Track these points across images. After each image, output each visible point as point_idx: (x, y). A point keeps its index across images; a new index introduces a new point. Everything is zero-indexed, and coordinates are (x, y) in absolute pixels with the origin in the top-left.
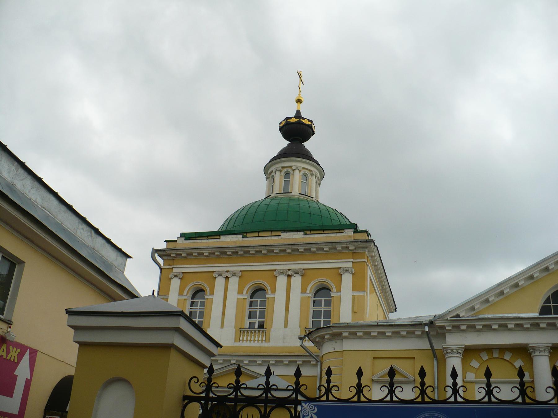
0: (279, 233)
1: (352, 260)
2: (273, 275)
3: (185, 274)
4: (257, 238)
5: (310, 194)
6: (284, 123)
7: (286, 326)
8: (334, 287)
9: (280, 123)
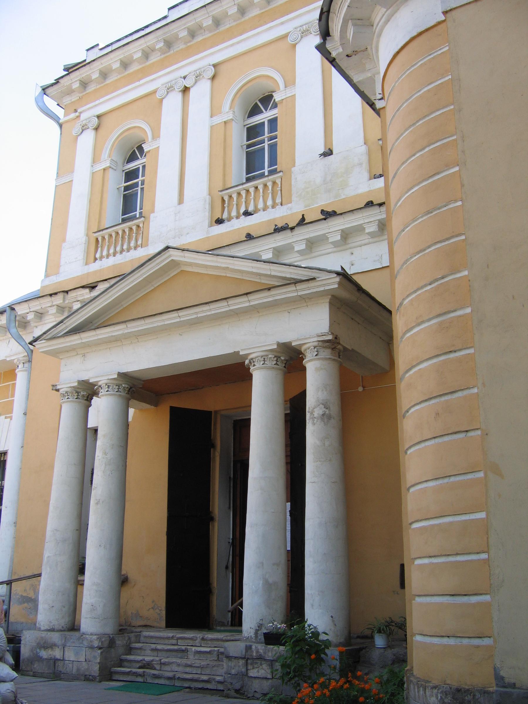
7: (181, 201)
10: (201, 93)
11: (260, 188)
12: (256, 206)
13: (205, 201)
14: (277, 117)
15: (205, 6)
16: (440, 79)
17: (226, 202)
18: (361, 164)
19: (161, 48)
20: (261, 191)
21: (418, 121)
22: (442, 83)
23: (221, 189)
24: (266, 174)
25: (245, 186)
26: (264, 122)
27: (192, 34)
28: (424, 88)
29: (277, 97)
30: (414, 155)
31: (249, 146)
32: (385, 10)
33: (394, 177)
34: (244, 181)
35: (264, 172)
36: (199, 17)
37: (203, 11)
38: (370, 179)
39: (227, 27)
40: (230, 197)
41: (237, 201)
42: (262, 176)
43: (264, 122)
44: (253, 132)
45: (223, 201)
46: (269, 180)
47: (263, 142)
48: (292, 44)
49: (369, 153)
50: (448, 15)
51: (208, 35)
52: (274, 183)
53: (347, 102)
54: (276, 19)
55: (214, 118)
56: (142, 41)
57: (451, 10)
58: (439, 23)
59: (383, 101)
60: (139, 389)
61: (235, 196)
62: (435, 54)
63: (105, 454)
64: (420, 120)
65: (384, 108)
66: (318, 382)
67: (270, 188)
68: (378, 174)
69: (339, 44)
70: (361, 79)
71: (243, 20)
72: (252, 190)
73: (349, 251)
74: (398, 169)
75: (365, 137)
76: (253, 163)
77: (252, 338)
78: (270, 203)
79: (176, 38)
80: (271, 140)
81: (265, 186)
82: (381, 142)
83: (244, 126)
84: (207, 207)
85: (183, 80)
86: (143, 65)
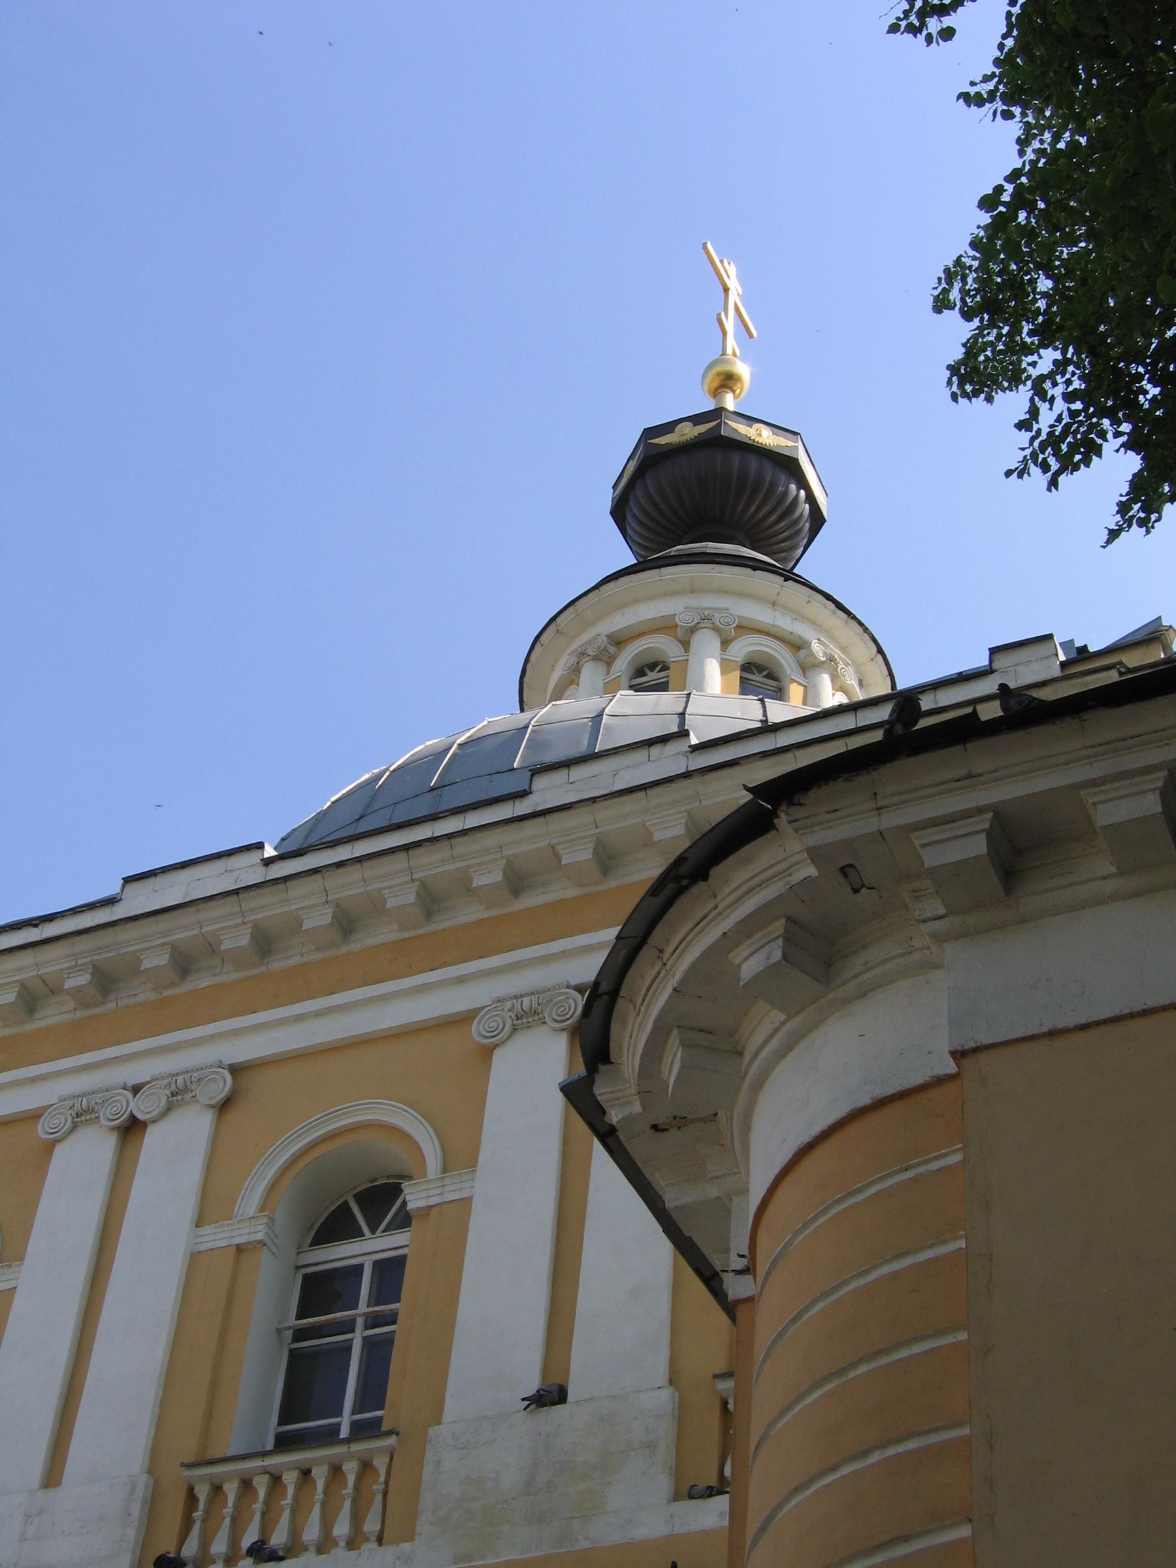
7: (52, 1476)
10: (178, 1149)
11: (320, 1475)
12: (295, 1532)
13: (133, 1489)
14: (404, 1257)
15: (236, 892)
16: (932, 1246)
17: (201, 1506)
18: (651, 1446)
19: (79, 989)
20: (320, 1485)
21: (854, 1365)
22: (935, 1260)
23: (189, 1459)
24: (344, 1433)
25: (270, 1461)
26: (361, 1266)
27: (184, 964)
28: (877, 1266)
29: (414, 1197)
30: (833, 1469)
31: (300, 1334)
32: (782, 1017)
33: (763, 1528)
34: (270, 1445)
35: (339, 1425)
36: (212, 920)
37: (230, 906)
38: (676, 1497)
39: (295, 960)
40: (217, 1489)
41: (237, 1507)
42: (330, 1436)
43: (361, 1266)
44: (322, 1291)
45: (191, 1498)
46: (351, 1456)
47: (349, 1326)
48: (483, 1045)
49: (682, 1414)
50: (967, 1062)
51: (231, 975)
52: (366, 1466)
53: (626, 1242)
54: (445, 965)
55: (207, 1230)
56: (27, 958)
57: (976, 1050)
58: (939, 1081)
59: (748, 1278)
61: (231, 1489)
62: (922, 1169)
64: (861, 1361)
65: (750, 1299)
67: (351, 1479)
68: (702, 1485)
69: (633, 1091)
70: (686, 1200)
71: (344, 949)
72: (290, 1479)
74: (779, 1507)
76: (306, 1387)
78: (342, 1528)
79: (133, 968)
80: (373, 1327)
81: (336, 1470)
82: (726, 1386)
83: (298, 1268)
84: (136, 1509)
85: (129, 1095)
86: (15, 1030)
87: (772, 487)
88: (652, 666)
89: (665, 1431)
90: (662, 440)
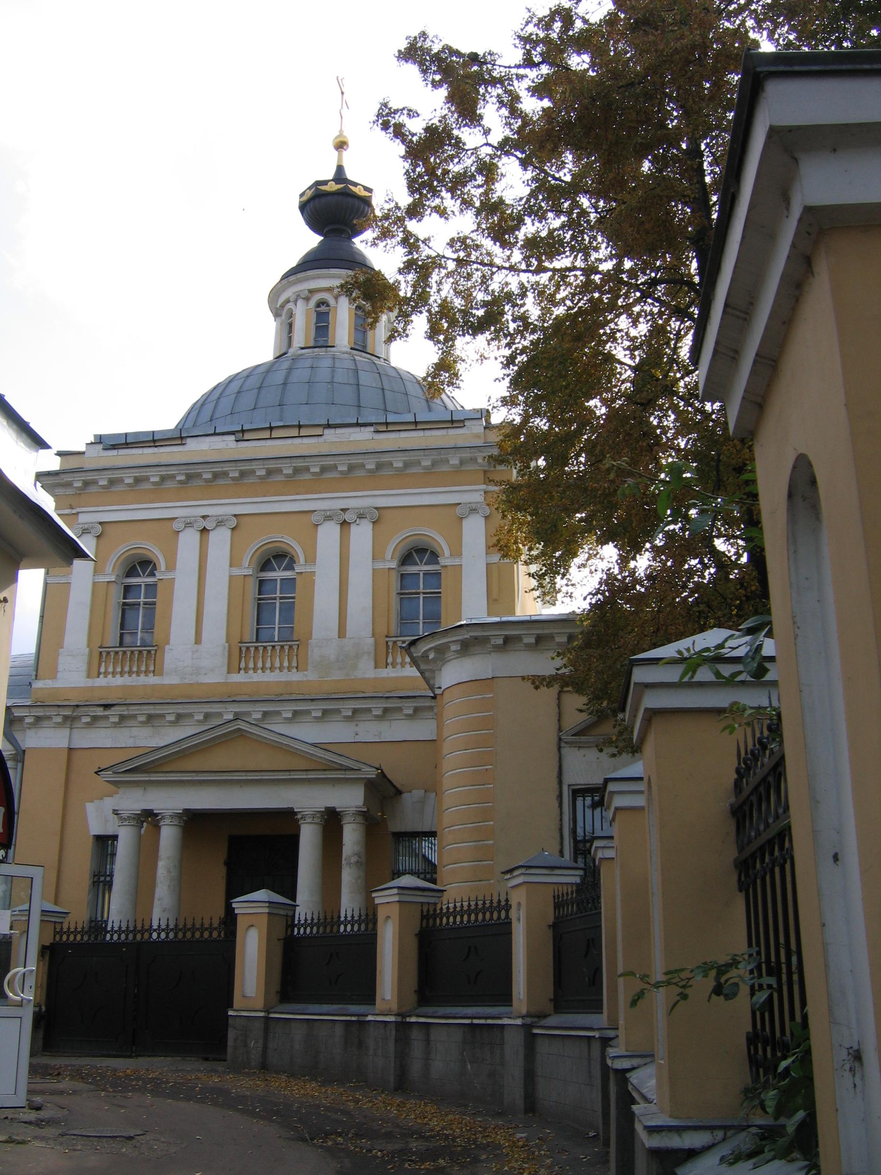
0: (319, 431)
1: (483, 487)
2: (309, 523)
3: (106, 526)
4: (270, 443)
5: (374, 350)
6: (309, 193)
7: (198, 640)
8: (162, 565)
9: (302, 195)
18: (369, 653)
23: (503, 870)
39: (251, 481)
49: (376, 644)
60: (194, 823)
63: (169, 872)
66: (352, 837)
73: (355, 723)
75: (373, 629)
77: (307, 800)
87: (363, 211)
88: (323, 303)
89: (372, 649)
90: (323, 188)
